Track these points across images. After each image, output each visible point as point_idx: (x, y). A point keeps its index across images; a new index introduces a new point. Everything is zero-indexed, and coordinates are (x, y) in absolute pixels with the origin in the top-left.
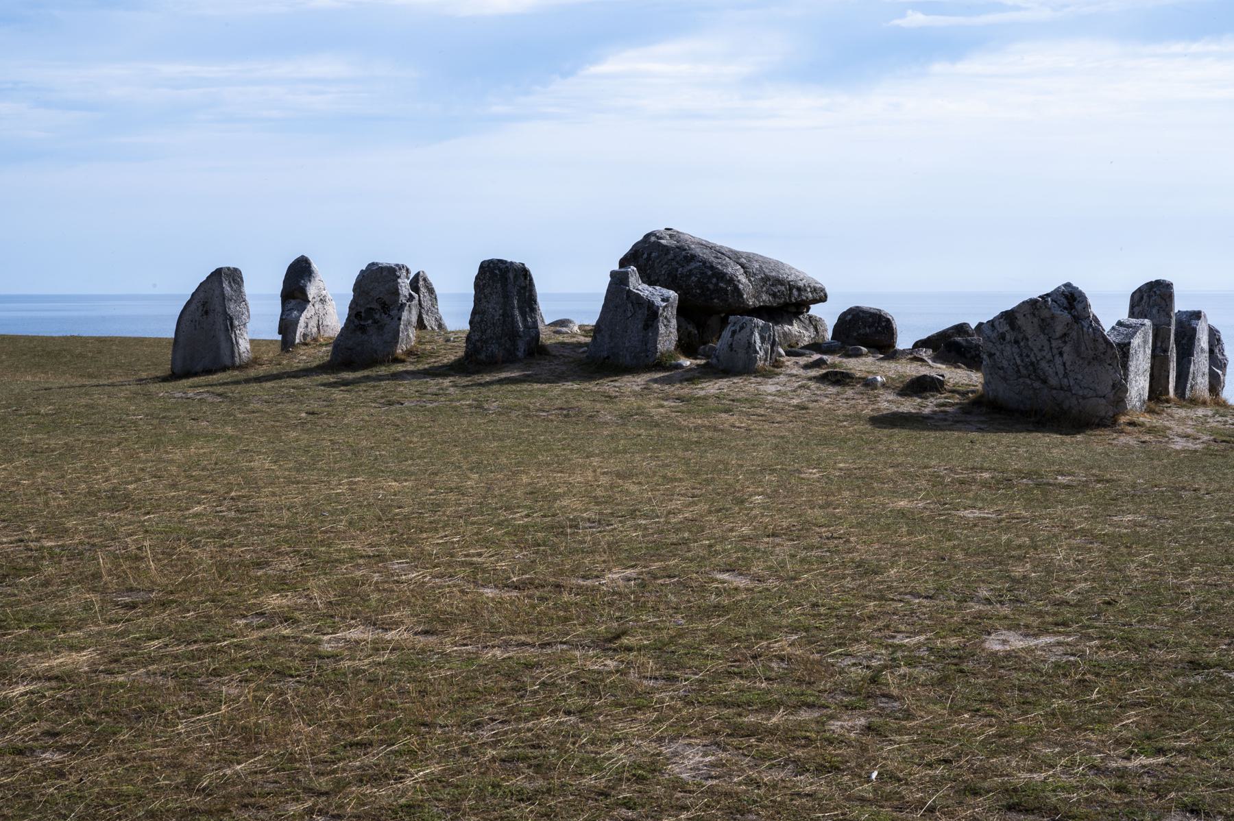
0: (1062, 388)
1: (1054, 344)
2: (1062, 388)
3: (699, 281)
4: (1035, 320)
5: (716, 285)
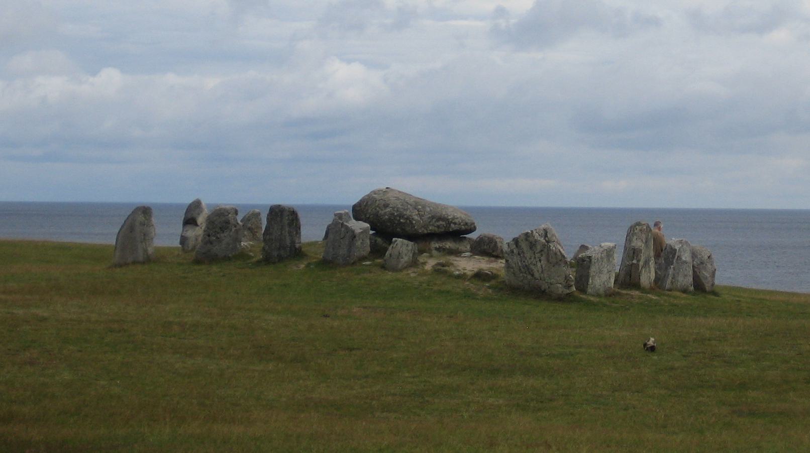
1: (537, 255)
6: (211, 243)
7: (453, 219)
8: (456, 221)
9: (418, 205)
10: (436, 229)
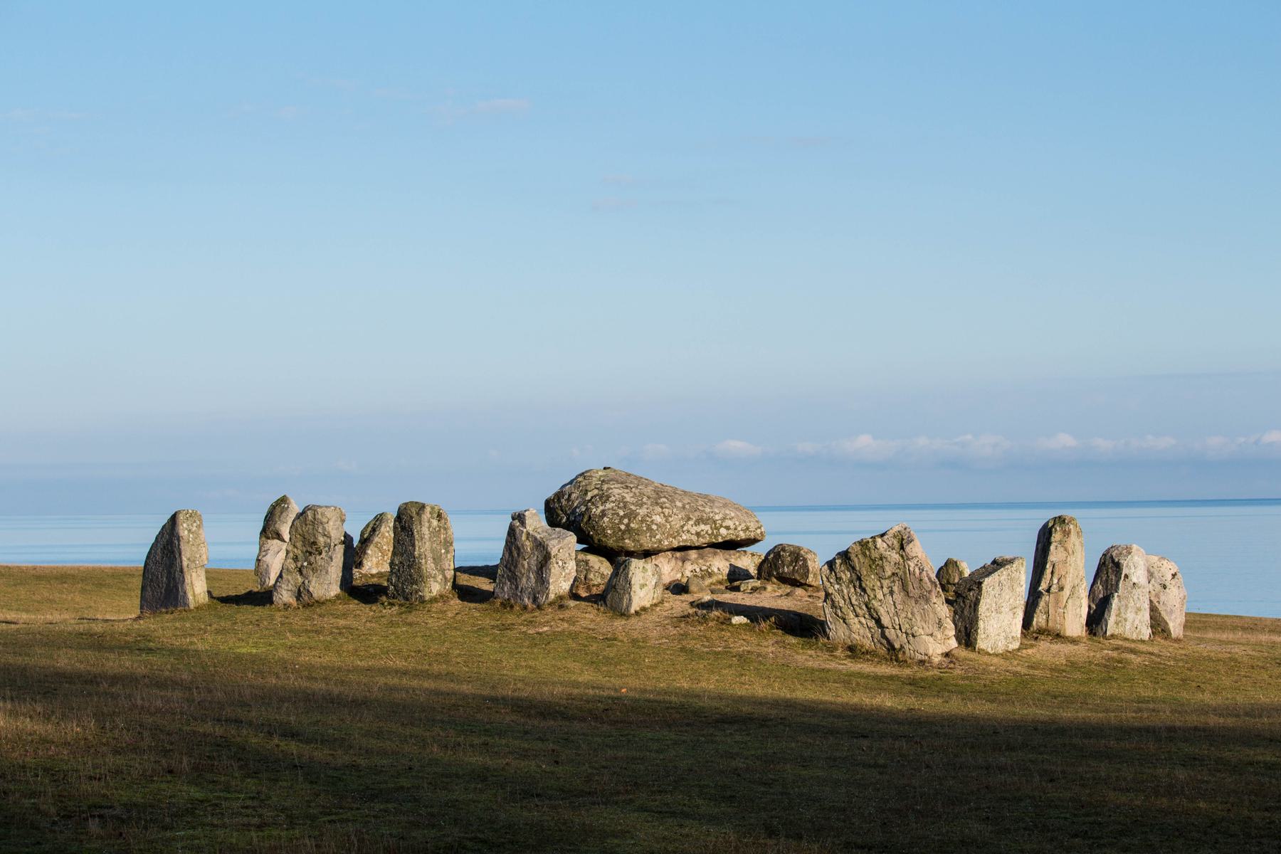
1: (886, 583)
10: (694, 538)
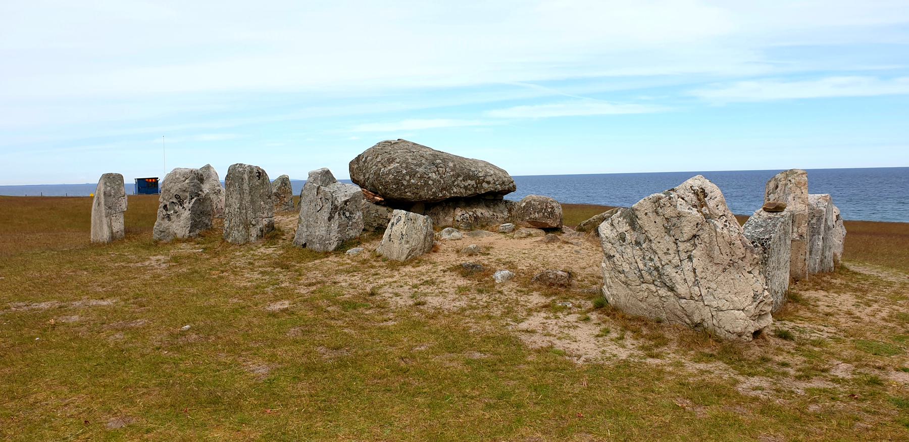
0: (692, 298)
1: (682, 246)
2: (692, 298)
3: (395, 178)
4: (658, 219)
5: (409, 181)
6: (169, 219)
7: (485, 176)
8: (489, 179)
9: (437, 159)
10: (463, 191)
